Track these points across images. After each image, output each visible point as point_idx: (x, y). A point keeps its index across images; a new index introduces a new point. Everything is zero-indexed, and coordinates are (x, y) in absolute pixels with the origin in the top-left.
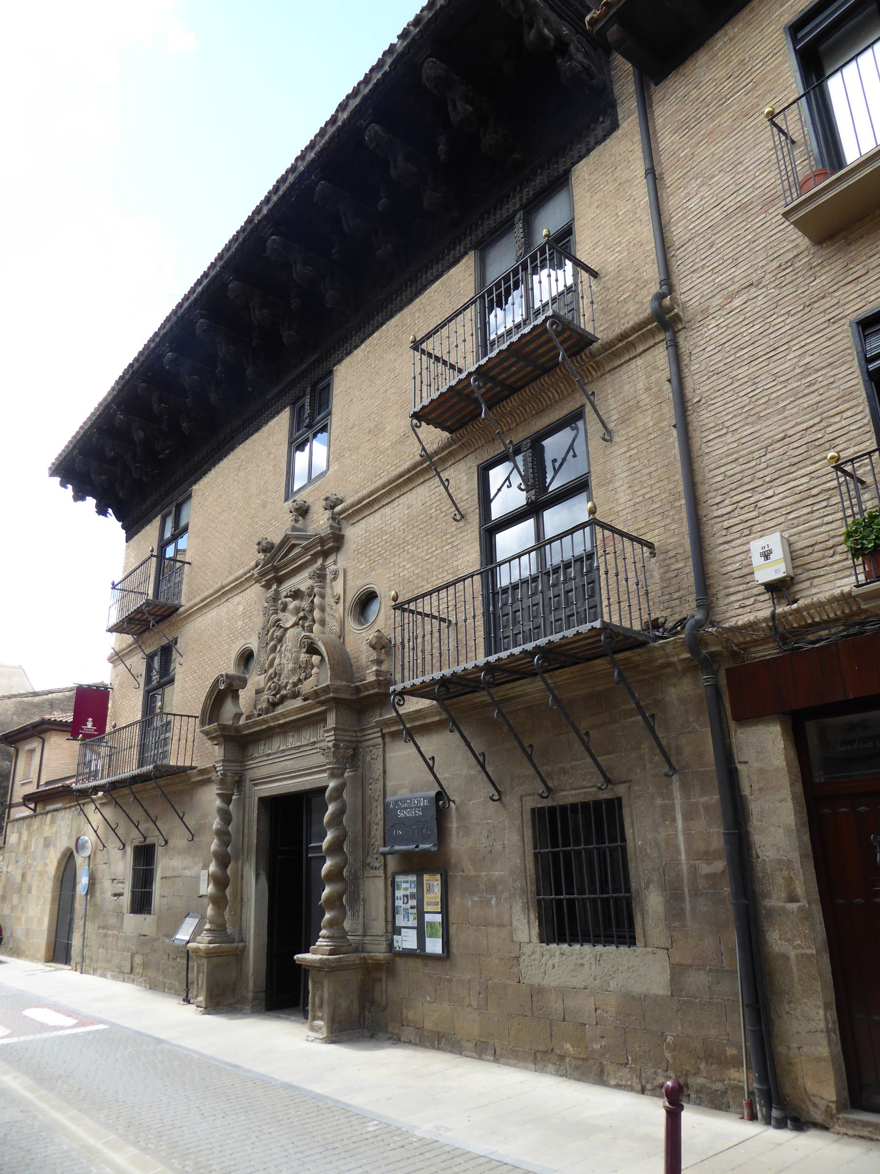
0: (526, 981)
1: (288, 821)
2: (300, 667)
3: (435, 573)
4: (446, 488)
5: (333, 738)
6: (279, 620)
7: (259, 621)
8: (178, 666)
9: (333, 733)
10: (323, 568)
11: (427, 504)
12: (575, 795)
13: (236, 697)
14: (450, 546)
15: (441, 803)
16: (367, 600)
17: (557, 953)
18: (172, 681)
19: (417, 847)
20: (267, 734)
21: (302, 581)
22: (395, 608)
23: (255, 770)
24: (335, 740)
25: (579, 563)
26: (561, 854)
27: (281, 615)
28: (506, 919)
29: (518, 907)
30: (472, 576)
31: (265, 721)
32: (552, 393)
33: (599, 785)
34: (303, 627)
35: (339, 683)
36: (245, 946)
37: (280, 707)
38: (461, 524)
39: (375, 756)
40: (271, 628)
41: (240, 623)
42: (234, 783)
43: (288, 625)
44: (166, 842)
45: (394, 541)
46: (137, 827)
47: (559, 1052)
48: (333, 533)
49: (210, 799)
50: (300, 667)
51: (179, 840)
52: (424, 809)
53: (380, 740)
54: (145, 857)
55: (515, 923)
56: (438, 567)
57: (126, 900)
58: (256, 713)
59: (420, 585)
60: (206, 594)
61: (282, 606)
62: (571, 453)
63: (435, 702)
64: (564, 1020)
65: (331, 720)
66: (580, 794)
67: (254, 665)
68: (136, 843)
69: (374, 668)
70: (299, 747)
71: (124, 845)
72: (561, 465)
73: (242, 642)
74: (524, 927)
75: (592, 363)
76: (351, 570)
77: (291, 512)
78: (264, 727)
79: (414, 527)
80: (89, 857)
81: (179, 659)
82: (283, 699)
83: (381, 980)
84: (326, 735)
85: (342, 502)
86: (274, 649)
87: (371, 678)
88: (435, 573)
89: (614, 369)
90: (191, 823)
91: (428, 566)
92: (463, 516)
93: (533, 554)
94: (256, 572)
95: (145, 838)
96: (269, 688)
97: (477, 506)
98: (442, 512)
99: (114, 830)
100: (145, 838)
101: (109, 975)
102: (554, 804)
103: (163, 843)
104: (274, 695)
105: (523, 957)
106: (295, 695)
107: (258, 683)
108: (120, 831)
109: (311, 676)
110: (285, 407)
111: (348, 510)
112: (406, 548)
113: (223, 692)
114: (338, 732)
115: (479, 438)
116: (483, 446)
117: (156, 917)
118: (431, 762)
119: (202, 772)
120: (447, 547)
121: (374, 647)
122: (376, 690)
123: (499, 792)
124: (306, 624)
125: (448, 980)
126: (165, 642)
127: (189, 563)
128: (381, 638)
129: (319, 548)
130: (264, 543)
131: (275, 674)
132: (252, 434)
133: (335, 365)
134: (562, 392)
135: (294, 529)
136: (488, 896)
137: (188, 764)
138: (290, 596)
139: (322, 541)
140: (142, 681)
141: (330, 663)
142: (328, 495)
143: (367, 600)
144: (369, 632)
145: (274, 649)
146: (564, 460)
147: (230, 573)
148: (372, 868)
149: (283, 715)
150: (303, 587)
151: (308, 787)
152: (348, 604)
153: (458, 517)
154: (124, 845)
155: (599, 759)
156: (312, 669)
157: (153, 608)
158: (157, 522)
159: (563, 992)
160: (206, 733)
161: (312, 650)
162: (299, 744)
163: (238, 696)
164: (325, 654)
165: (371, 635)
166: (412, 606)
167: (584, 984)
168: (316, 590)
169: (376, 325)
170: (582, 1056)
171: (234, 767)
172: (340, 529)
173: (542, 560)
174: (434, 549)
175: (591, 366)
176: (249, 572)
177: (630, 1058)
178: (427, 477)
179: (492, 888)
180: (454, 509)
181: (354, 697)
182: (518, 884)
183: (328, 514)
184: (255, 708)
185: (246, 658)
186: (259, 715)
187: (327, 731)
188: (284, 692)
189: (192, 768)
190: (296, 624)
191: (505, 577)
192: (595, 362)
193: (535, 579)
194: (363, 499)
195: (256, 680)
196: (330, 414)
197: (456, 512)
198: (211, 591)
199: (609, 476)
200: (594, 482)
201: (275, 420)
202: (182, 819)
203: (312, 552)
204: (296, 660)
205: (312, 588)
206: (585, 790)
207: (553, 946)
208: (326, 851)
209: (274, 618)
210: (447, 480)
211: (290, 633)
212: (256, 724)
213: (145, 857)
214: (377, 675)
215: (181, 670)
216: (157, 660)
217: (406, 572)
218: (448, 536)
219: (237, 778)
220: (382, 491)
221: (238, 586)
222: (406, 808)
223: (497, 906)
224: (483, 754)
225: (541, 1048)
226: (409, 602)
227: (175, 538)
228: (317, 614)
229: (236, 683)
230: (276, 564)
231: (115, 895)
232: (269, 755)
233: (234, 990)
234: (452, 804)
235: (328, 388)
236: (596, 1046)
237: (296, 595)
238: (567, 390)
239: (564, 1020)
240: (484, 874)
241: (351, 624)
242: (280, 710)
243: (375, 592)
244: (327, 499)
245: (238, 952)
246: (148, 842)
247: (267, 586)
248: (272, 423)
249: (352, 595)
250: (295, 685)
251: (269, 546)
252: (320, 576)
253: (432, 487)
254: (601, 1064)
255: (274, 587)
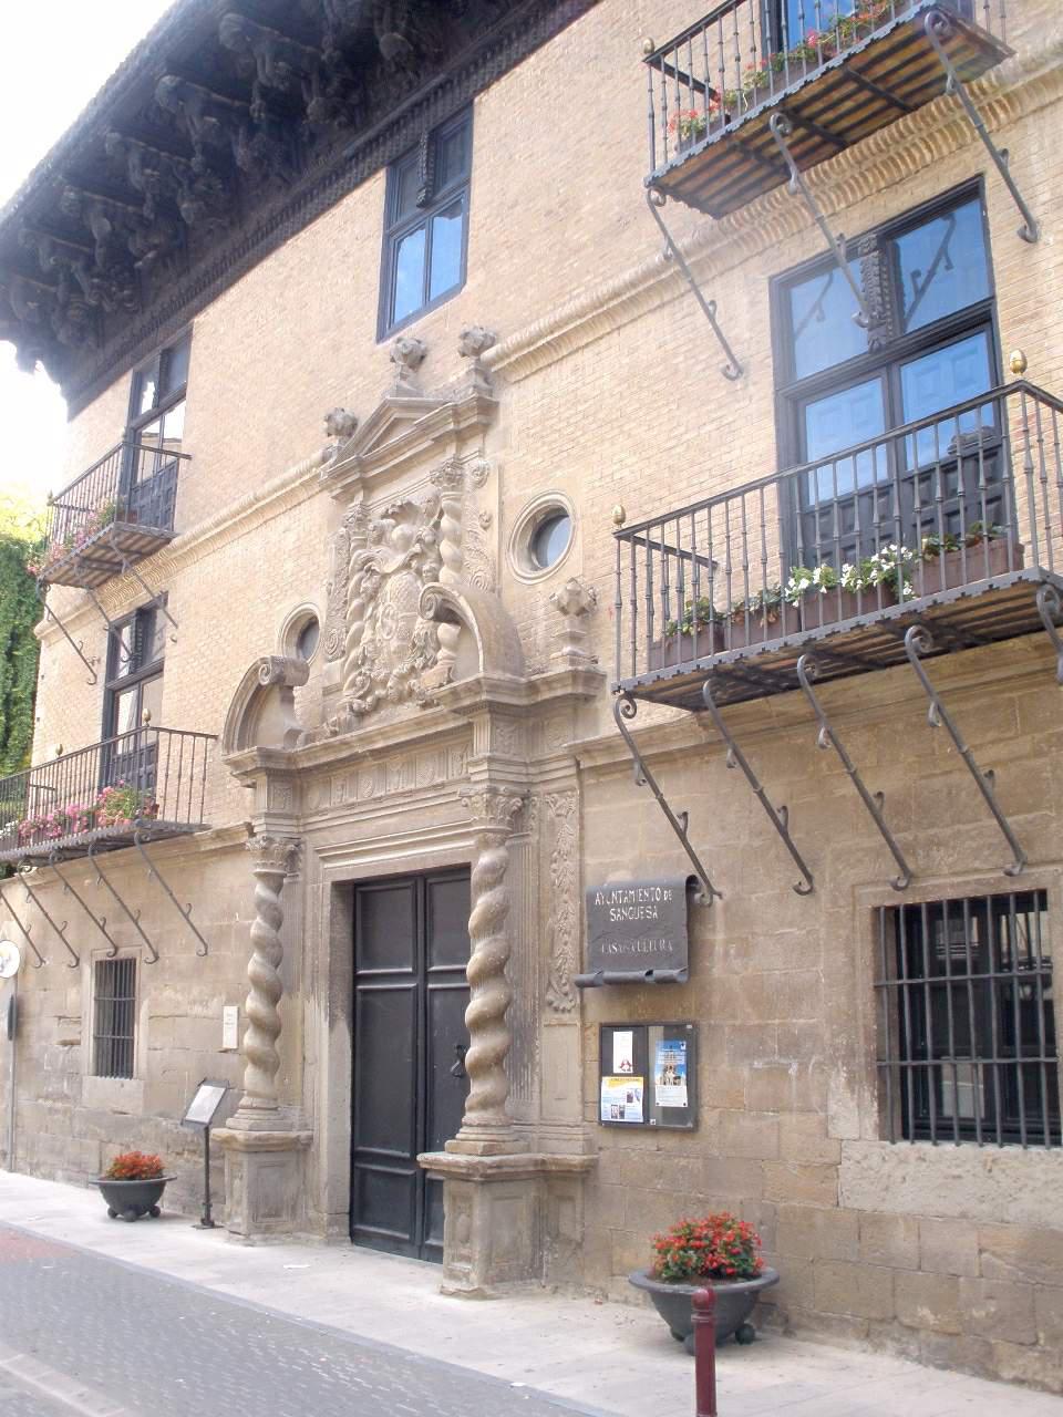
0: (849, 1204)
1: (394, 924)
2: (414, 645)
3: (685, 474)
4: (711, 318)
5: (486, 776)
6: (369, 559)
7: (327, 561)
8: (169, 643)
9: (485, 767)
10: (457, 463)
11: (669, 347)
12: (959, 884)
13: (288, 700)
14: (714, 426)
15: (697, 896)
16: (545, 524)
17: (912, 1158)
18: (158, 671)
19: (649, 973)
20: (347, 766)
21: (416, 486)
22: (620, 536)
23: (325, 834)
24: (490, 780)
25: (971, 464)
26: (927, 988)
27: (374, 551)
28: (815, 1099)
29: (839, 1079)
30: (760, 485)
31: (345, 743)
32: (920, 151)
33: (1008, 866)
34: (419, 572)
35: (497, 675)
36: (311, 1138)
37: (375, 718)
38: (739, 385)
39: (563, 812)
40: (354, 572)
41: (289, 566)
42: (287, 864)
43: (388, 569)
44: (157, 958)
45: (601, 416)
46: (103, 929)
47: (907, 1321)
48: (479, 399)
49: (238, 887)
50: (414, 645)
51: (179, 951)
52: (663, 907)
53: (574, 782)
54: (117, 980)
55: (833, 1107)
56: (692, 464)
57: (87, 1051)
58: (327, 729)
59: (656, 495)
60: (224, 512)
61: (375, 534)
62: (943, 264)
63: (685, 713)
64: (920, 1268)
65: (482, 742)
66: (967, 883)
67: (320, 642)
68: (102, 956)
69: (567, 649)
70: (411, 792)
71: (78, 960)
72: (928, 281)
73: (297, 600)
74: (852, 1112)
75: (1000, 97)
76: (515, 465)
77: (393, 360)
78: (344, 754)
79: (641, 388)
80: (16, 976)
81: (170, 631)
82: (378, 704)
83: (571, 1199)
84: (471, 770)
85: (493, 342)
86: (362, 609)
87: (562, 668)
88: (685, 474)
89: (1042, 108)
90: (203, 921)
91: (671, 462)
92: (735, 371)
93: (881, 450)
94: (323, 472)
95: (116, 949)
96: (353, 684)
97: (770, 352)
98: (697, 363)
99: (60, 933)
100: (116, 949)
101: (60, 1173)
102: (917, 900)
103: (152, 958)
104: (362, 697)
105: (846, 1164)
106: (401, 698)
107: (328, 674)
108: (70, 936)
109: (435, 662)
110: (374, 171)
111: (508, 356)
112: (626, 428)
113: (266, 690)
114: (495, 766)
115: (774, 228)
116: (780, 242)
117: (142, 1083)
118: (681, 823)
119: (220, 834)
120: (708, 428)
121: (564, 611)
122: (569, 690)
123: (809, 877)
124: (426, 567)
125: (699, 1200)
126: (143, 599)
127: (188, 457)
128: (579, 593)
129: (452, 426)
130: (339, 418)
131: (365, 657)
132: (311, 221)
133: (477, 93)
134: (939, 148)
135: (399, 391)
136: (783, 1061)
137: (195, 819)
138: (393, 515)
139: (456, 413)
140: (101, 670)
141: (482, 640)
142: (467, 328)
143: (545, 524)
144: (555, 582)
145: (362, 609)
146: (932, 273)
147: (269, 475)
148: (556, 1010)
149: (382, 734)
150: (418, 498)
151: (430, 865)
152: (508, 532)
153: (732, 372)
154: (78, 960)
155: (1009, 820)
156: (438, 648)
157: (128, 538)
158: (125, 384)
159: (917, 1222)
160: (235, 764)
161: (447, 614)
162: (412, 787)
163: (293, 698)
164: (472, 620)
165: (559, 589)
166: (655, 534)
167: (959, 1209)
168: (444, 503)
169: (559, 22)
170: (952, 1329)
171: (286, 828)
172: (491, 392)
173: (898, 459)
174: (682, 429)
175: (998, 101)
176: (309, 471)
177: (1041, 1335)
178: (667, 297)
179: (792, 1045)
180: (723, 355)
181: (524, 702)
182: (842, 1040)
183: (467, 364)
184: (324, 719)
185: (304, 630)
186: (335, 734)
187: (476, 763)
188: (380, 692)
189: (202, 827)
190: (406, 566)
191: (825, 487)
192: (1007, 96)
193: (884, 490)
194: (540, 336)
195: (323, 669)
196: (468, 182)
197: (729, 362)
198: (235, 506)
199: (1031, 304)
200: (1002, 314)
201: (357, 193)
202: (186, 916)
203: (437, 435)
204: (406, 635)
205: (437, 499)
206: (976, 877)
207: (904, 1145)
208: (473, 978)
209: (362, 553)
210: (713, 303)
211: (391, 585)
212: (327, 748)
213: (117, 980)
214: (572, 662)
215: (176, 650)
216: (126, 635)
217: (626, 472)
218: (712, 406)
219: (291, 847)
220: (578, 322)
221: (287, 498)
222: (626, 906)
223: (798, 1078)
224: (785, 808)
225: (874, 1315)
226: (648, 526)
227: (161, 409)
228: (446, 548)
229: (291, 673)
230: (360, 455)
231: (65, 1043)
232: (352, 806)
233: (294, 1208)
234: (716, 898)
235: (465, 129)
236: (978, 1313)
237: (404, 512)
238: (949, 146)
239: (920, 1268)
240: (777, 1021)
241: (516, 565)
242: (372, 725)
243: (562, 509)
244: (465, 335)
245: (300, 1147)
246: (123, 953)
247: (345, 496)
248: (349, 201)
249: (517, 515)
250: (403, 678)
251: (350, 423)
252: (453, 478)
253: (679, 316)
254: (987, 1343)
255: (360, 497)
